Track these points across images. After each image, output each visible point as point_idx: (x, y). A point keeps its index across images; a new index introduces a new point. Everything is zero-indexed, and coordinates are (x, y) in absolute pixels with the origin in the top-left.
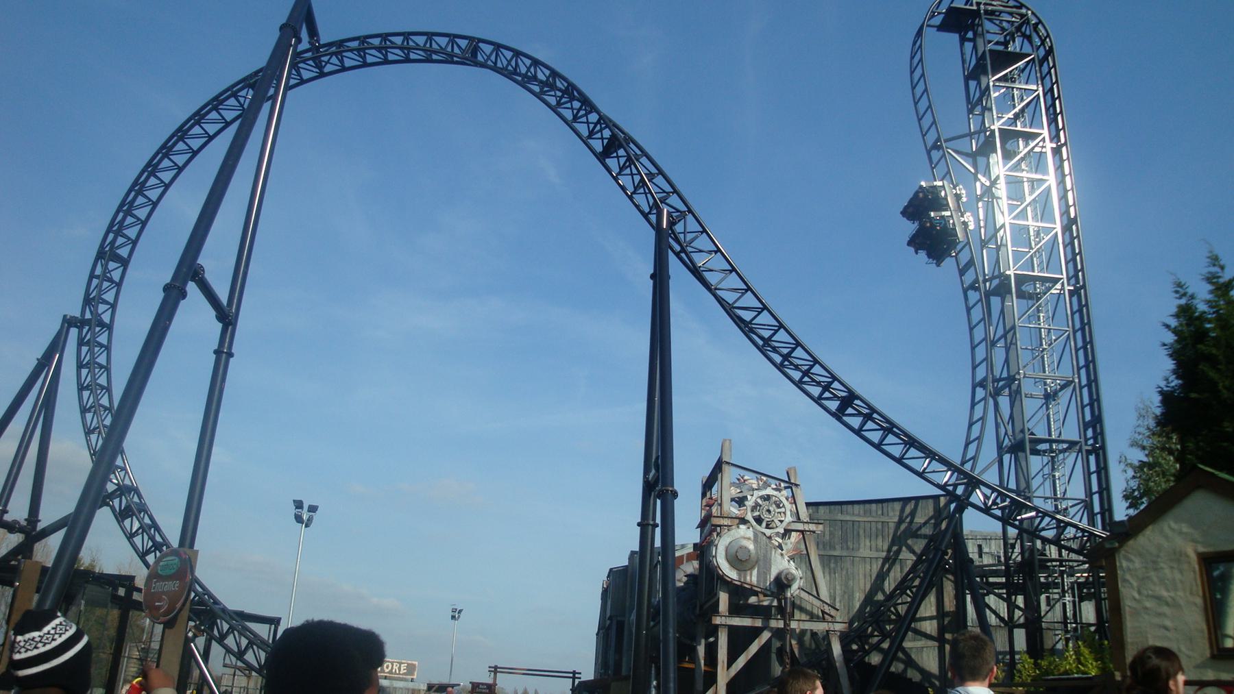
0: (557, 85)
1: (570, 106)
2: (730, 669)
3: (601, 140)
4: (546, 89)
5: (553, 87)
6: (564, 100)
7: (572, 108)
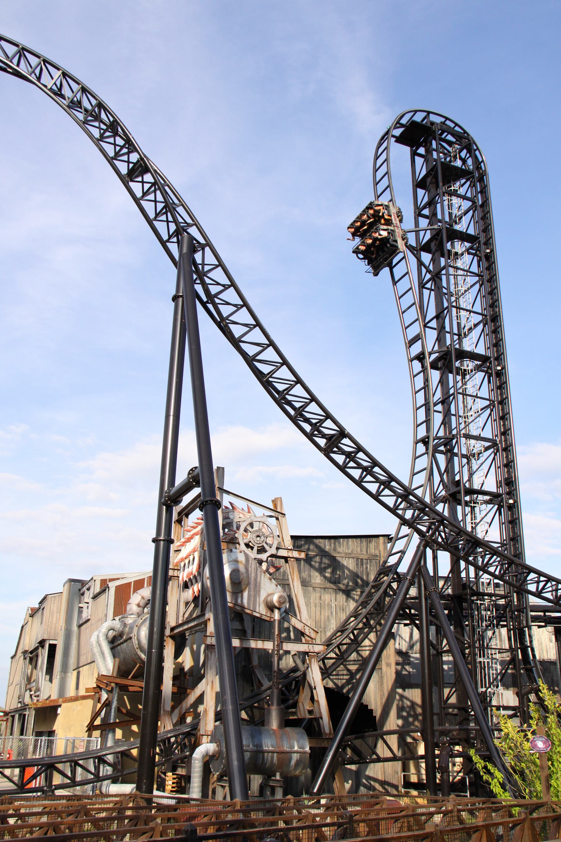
0: (102, 116)
1: (113, 142)
2: (201, 692)
3: (141, 184)
4: (90, 118)
5: (97, 118)
6: (108, 134)
7: (115, 145)
